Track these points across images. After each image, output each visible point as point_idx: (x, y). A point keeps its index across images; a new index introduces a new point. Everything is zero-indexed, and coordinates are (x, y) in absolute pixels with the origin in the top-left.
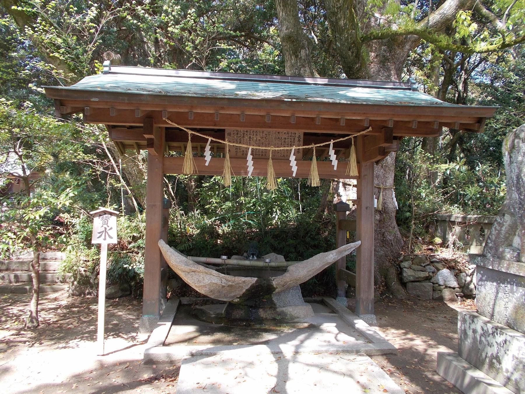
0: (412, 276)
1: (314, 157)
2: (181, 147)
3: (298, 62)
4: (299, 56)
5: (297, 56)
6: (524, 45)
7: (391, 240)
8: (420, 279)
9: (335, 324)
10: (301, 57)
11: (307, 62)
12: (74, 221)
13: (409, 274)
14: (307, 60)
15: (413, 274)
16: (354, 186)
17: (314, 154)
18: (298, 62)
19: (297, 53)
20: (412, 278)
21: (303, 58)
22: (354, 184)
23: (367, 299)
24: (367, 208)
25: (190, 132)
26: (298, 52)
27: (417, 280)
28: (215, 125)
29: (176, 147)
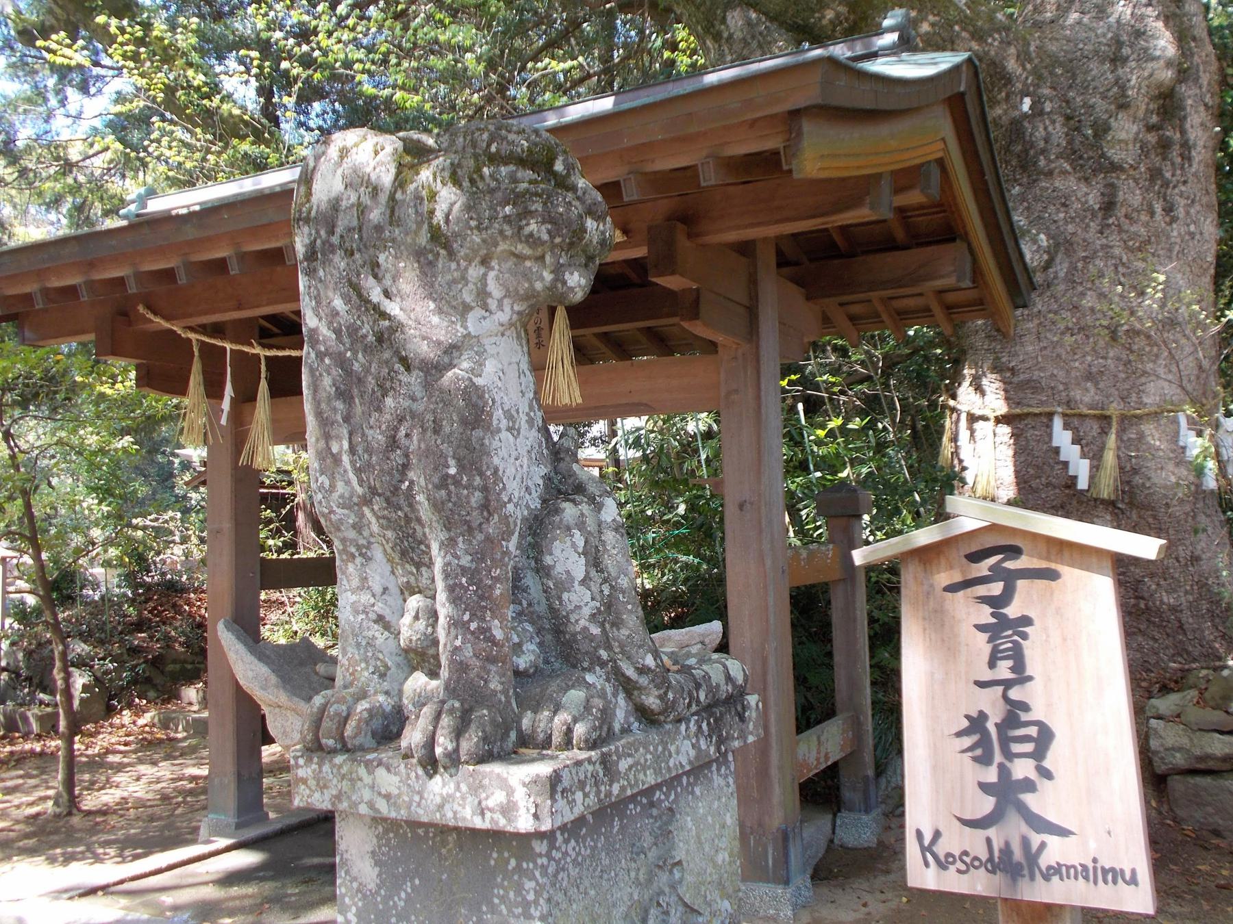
0: (1180, 749)
1: (263, 386)
2: (930, 310)
3: (727, 51)
4: (725, 35)
5: (717, 37)
6: (660, 1)
7: (1174, 609)
8: (1211, 764)
9: (43, 858)
10: (731, 36)
11: (754, 44)
12: (354, 598)
13: (1170, 741)
14: (753, 37)
15: (1185, 741)
16: (998, 420)
17: (263, 375)
18: (727, 51)
19: (713, 26)
20: (1179, 760)
21: (738, 35)
22: (999, 413)
23: (760, 825)
24: (741, 506)
25: (192, 336)
26: (717, 23)
27: (1202, 766)
28: (239, 307)
29: (918, 312)
